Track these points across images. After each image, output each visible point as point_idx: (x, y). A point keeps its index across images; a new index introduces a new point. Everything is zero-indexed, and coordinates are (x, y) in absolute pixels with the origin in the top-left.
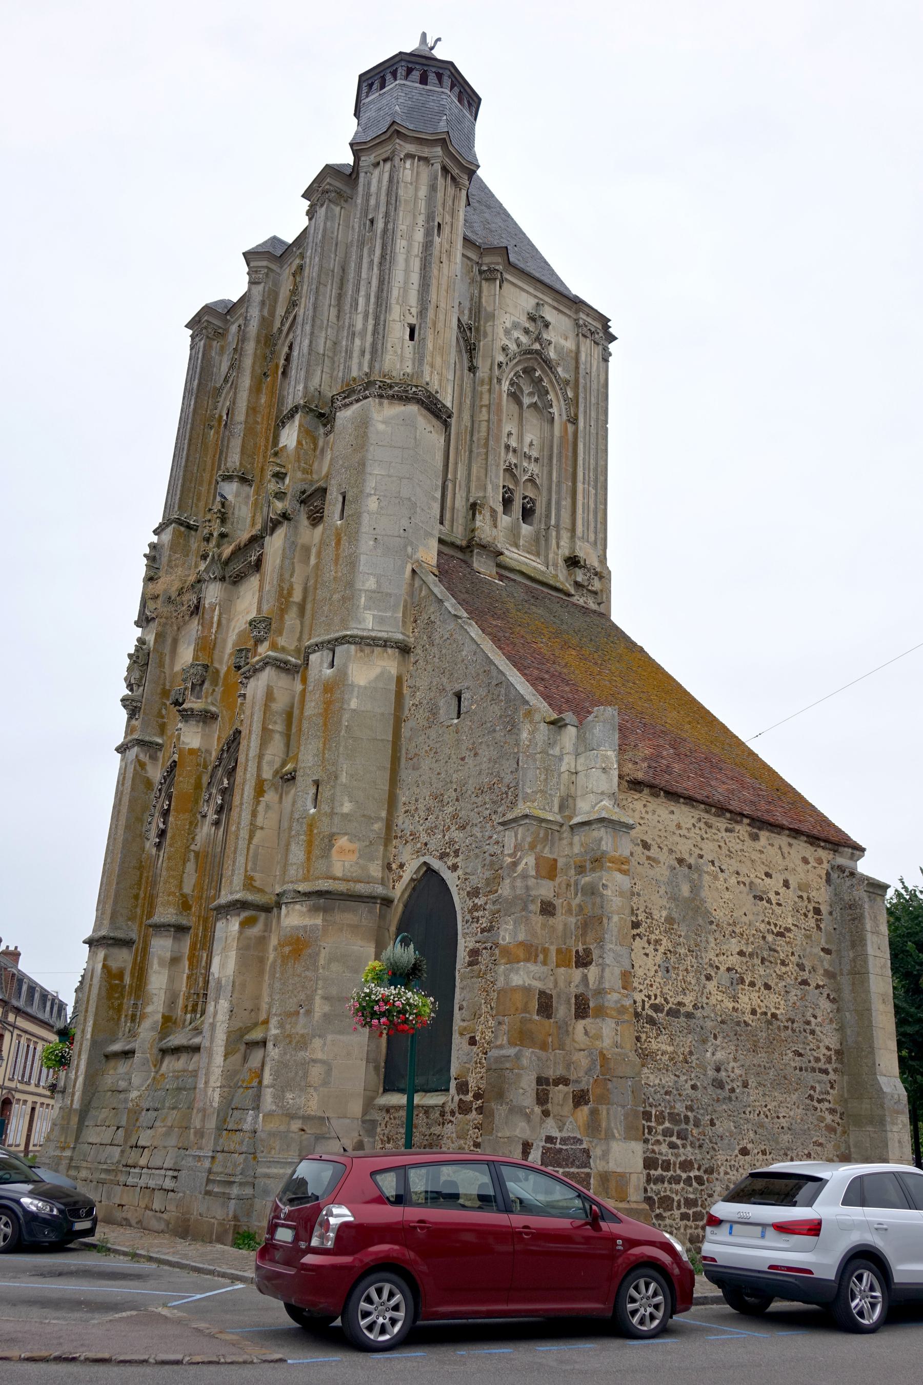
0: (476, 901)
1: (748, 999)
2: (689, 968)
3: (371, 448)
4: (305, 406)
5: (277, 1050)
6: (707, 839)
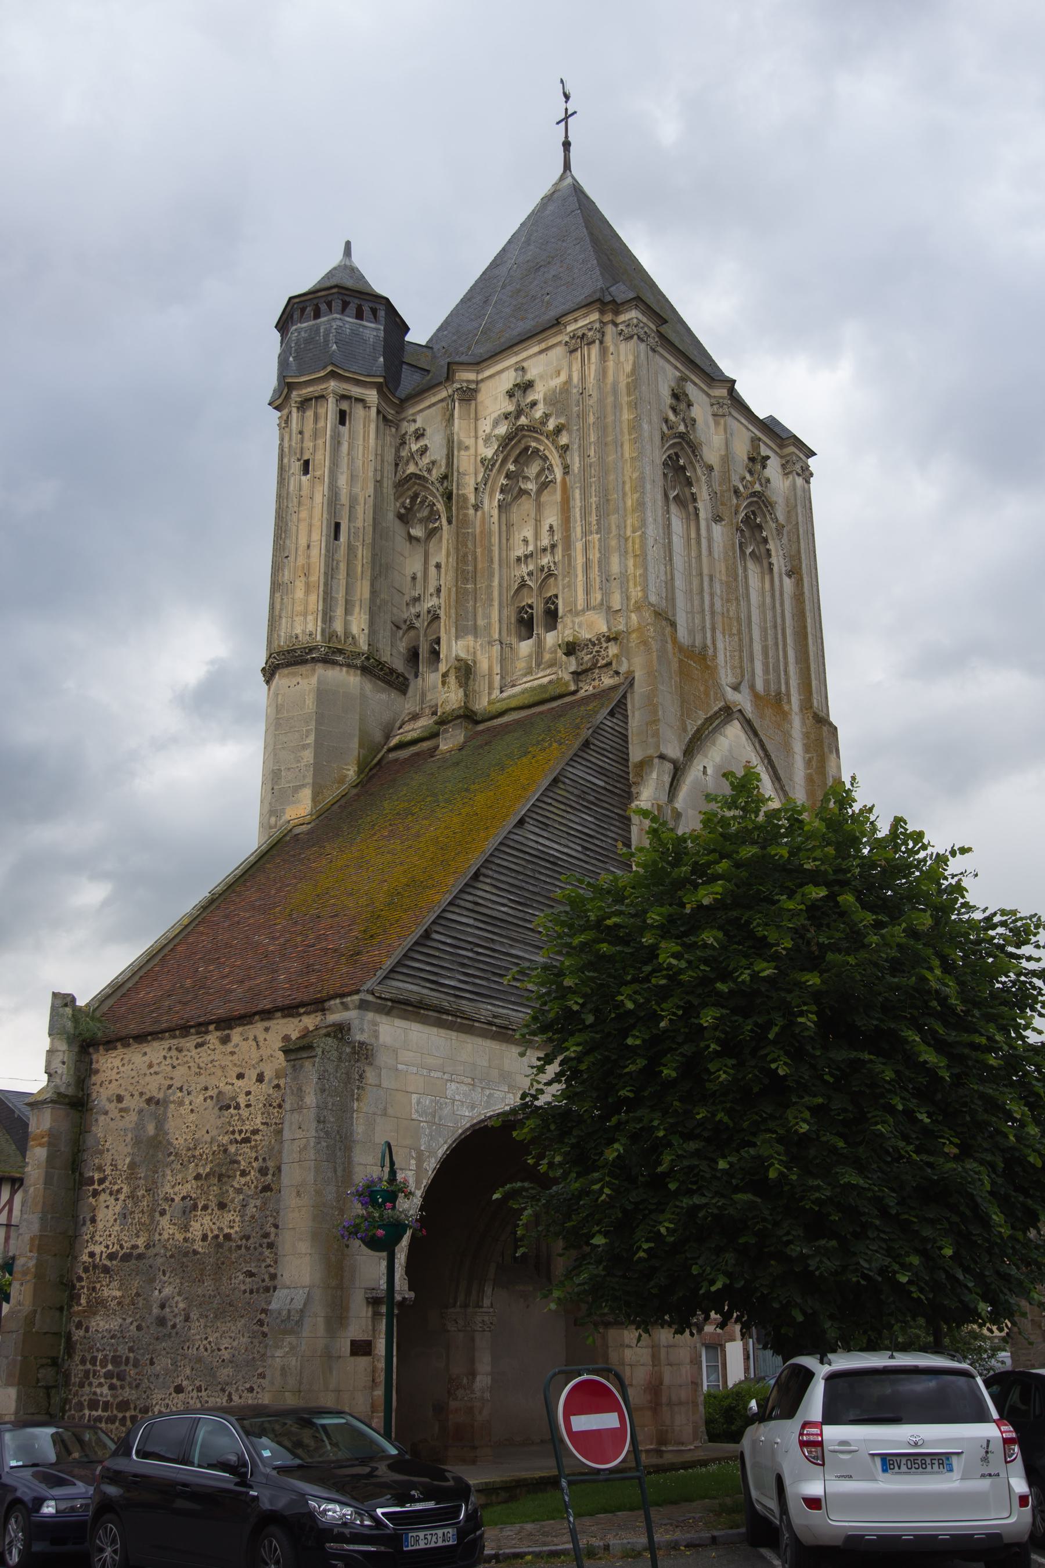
1: (201, 1224)
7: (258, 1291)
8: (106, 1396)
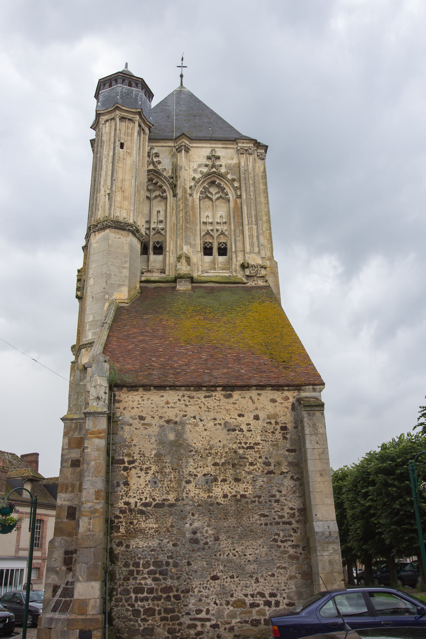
2: (173, 479)
6: (191, 405)
7: (271, 524)
8: (151, 585)
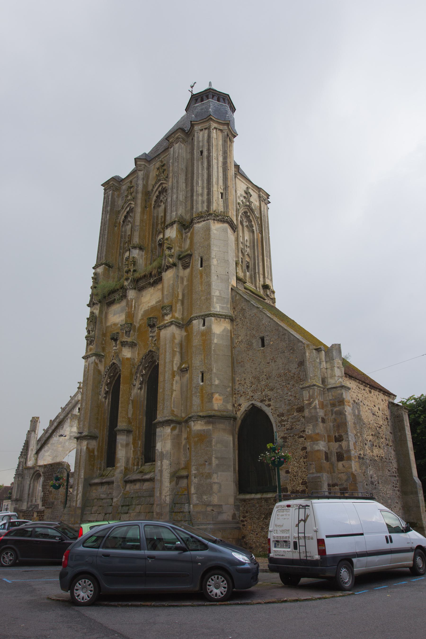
0: (283, 418)
1: (376, 451)
3: (212, 240)
4: (178, 221)
5: (196, 479)
